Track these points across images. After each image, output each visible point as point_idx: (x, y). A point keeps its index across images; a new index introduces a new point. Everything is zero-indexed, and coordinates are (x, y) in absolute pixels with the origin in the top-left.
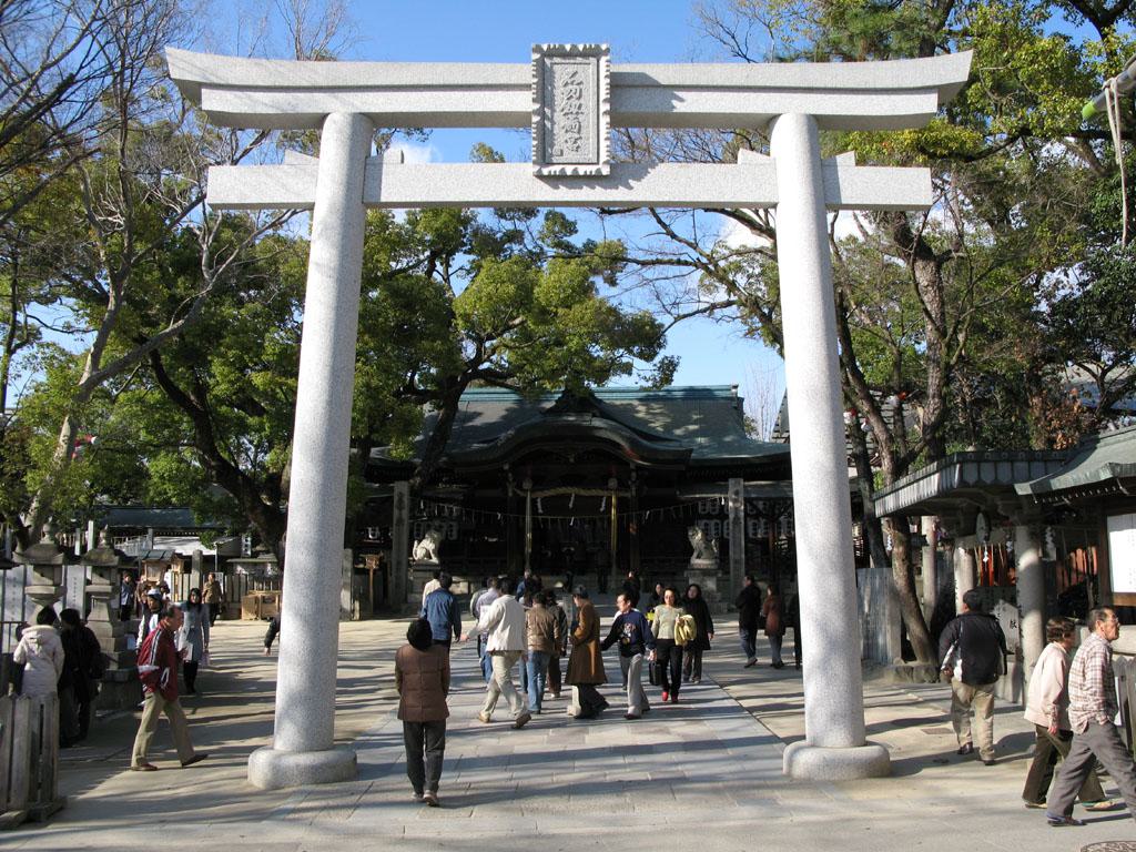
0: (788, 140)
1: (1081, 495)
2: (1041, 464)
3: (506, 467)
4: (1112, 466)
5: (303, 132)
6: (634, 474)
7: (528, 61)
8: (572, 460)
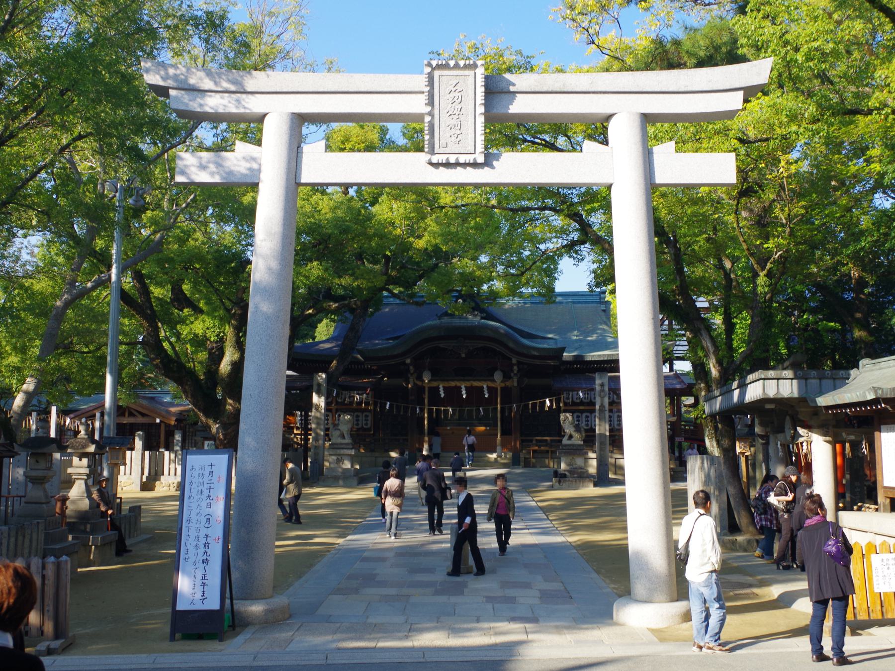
0: (624, 132)
1: (856, 409)
2: (831, 382)
3: (408, 361)
4: (875, 389)
6: (515, 368)
7: (421, 73)
8: (463, 355)
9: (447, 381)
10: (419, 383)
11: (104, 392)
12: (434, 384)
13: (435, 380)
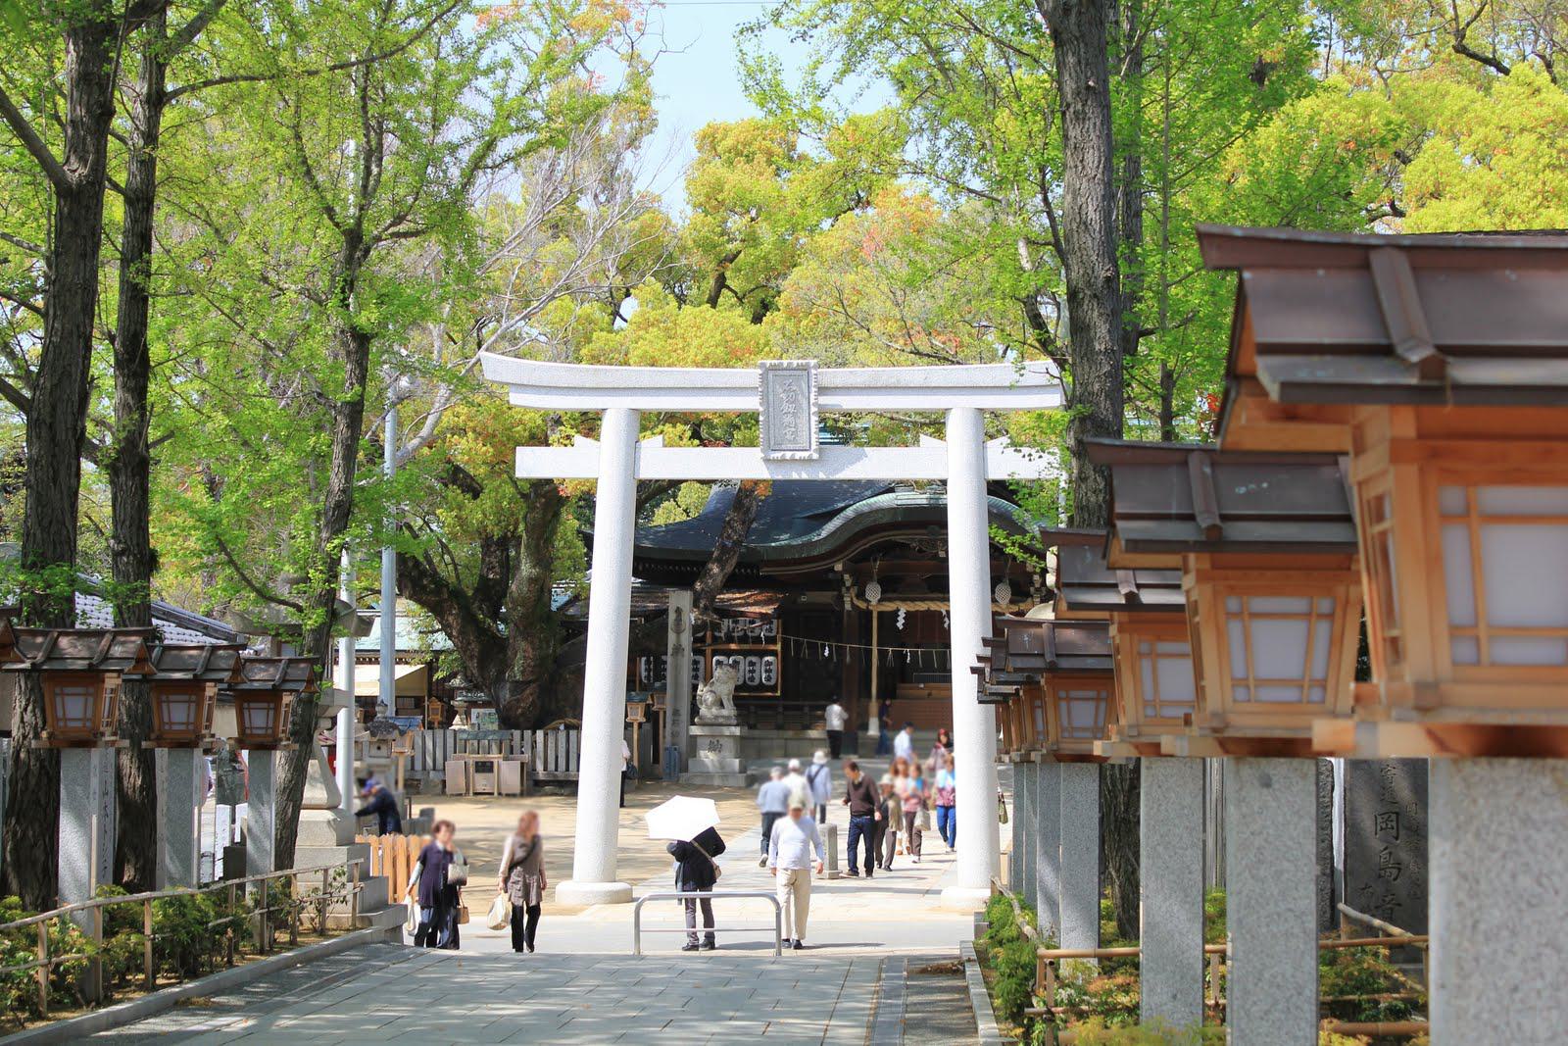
5: (589, 424)
9: (913, 600)
10: (862, 605)
11: (940, 586)
12: (889, 607)
13: (890, 600)
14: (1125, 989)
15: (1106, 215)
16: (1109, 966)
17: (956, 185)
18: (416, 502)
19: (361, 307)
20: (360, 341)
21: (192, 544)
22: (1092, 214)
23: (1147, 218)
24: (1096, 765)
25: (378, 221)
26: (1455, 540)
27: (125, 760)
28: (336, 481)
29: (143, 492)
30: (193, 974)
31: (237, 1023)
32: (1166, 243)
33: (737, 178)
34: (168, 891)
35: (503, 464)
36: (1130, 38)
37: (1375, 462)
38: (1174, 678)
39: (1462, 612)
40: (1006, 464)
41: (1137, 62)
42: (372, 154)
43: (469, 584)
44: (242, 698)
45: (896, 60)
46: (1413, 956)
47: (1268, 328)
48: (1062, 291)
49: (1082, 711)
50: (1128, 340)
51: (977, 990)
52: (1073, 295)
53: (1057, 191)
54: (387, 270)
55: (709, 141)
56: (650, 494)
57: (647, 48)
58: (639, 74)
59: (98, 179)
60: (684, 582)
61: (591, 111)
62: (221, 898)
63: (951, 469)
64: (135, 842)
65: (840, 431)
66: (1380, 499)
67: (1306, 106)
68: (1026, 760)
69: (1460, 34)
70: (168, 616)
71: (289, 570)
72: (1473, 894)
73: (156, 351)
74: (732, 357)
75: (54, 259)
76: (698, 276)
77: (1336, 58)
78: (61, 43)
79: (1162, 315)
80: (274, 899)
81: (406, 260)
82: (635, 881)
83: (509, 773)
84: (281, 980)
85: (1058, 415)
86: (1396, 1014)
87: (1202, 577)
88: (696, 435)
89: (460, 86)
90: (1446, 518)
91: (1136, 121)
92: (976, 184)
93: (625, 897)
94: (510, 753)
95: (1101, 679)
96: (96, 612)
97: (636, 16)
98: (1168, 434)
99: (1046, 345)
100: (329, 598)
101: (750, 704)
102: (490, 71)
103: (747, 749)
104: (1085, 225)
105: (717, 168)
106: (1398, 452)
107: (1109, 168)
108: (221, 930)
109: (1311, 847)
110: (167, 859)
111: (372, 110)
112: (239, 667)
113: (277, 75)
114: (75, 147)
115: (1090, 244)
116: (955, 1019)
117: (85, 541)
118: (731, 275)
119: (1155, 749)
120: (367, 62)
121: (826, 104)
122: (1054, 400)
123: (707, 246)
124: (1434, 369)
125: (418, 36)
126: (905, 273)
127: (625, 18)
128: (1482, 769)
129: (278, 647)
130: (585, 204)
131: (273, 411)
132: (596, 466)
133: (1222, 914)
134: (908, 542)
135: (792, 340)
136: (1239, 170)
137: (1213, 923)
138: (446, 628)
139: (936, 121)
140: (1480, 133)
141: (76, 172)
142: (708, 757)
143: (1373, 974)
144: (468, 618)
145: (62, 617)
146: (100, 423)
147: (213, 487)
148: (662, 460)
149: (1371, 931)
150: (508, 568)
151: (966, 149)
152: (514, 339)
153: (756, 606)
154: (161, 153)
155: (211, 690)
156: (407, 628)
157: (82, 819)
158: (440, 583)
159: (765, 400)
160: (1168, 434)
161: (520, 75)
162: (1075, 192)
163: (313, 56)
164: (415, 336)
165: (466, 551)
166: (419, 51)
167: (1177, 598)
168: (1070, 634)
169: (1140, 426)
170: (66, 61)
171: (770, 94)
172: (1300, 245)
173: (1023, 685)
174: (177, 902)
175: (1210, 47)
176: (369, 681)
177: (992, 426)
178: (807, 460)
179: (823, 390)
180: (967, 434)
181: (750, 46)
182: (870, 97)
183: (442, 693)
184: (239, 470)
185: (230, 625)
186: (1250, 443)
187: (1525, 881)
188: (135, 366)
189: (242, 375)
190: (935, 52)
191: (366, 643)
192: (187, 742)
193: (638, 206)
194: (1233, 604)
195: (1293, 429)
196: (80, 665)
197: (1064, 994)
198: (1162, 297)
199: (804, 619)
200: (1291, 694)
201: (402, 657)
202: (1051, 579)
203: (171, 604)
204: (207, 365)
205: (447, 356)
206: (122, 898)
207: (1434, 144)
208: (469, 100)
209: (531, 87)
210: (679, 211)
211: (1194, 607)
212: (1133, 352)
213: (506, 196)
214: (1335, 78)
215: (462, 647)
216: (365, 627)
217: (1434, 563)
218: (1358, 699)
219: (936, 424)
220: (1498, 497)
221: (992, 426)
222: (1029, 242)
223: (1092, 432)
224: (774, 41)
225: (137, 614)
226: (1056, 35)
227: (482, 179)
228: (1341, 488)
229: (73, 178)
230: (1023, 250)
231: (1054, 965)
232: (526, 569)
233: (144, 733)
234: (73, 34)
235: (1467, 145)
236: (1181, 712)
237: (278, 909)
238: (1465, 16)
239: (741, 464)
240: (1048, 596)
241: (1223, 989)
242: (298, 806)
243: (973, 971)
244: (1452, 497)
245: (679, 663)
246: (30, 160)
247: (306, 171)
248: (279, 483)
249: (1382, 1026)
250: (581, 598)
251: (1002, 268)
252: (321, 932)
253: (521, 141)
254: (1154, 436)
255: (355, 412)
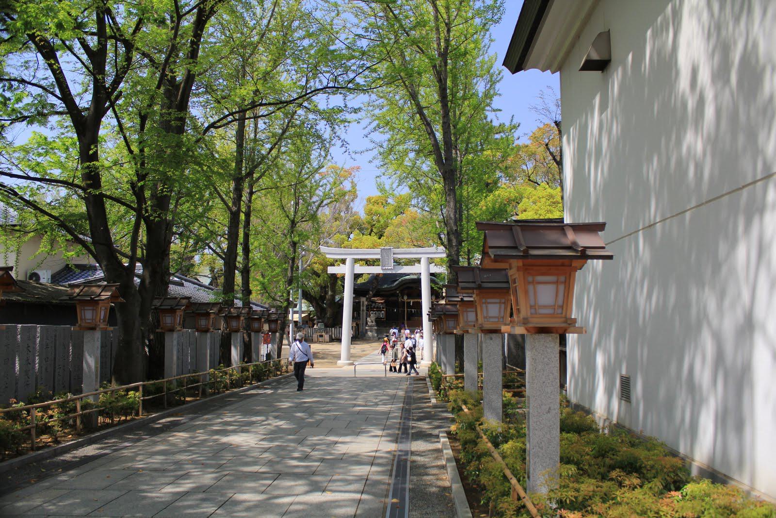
5: (343, 261)
11: (419, 296)
12: (409, 300)
14: (461, 383)
15: (455, 216)
16: (457, 378)
17: (422, 209)
18: (306, 278)
19: (294, 237)
20: (294, 244)
21: (258, 288)
22: (452, 216)
23: (464, 216)
24: (454, 339)
25: (298, 218)
26: (531, 288)
27: (245, 335)
28: (289, 274)
29: (248, 278)
30: (260, 381)
31: (269, 392)
32: (468, 222)
33: (375, 208)
34: (254, 363)
35: (325, 270)
36: (459, 178)
37: (514, 272)
38: (471, 316)
39: (532, 303)
40: (434, 269)
41: (461, 182)
42: (297, 204)
43: (318, 297)
44: (269, 321)
45: (410, 183)
46: (522, 375)
47: (491, 243)
48: (446, 232)
49: (451, 323)
50: (460, 243)
51: (429, 384)
52: (448, 234)
53: (444, 211)
54: (300, 229)
55: (369, 200)
56: (357, 276)
57: (355, 180)
58: (354, 186)
59: (239, 210)
60: (364, 296)
61: (344, 194)
62: (266, 365)
63: (422, 270)
64: (248, 353)
65: (398, 262)
66: (515, 279)
67: (497, 193)
68: (439, 334)
69: (529, 177)
70: (254, 304)
71: (279, 294)
72: (535, 363)
73: (251, 247)
74: (374, 247)
75: (230, 228)
76: (367, 229)
77: (504, 182)
78: (231, 182)
79: (467, 238)
80: (277, 365)
81: (304, 226)
82: (354, 361)
83: (327, 337)
84: (279, 382)
85: (445, 259)
86: (519, 387)
87: (477, 295)
88: (366, 263)
89: (316, 189)
90: (529, 283)
91: (461, 196)
92: (427, 209)
93: (352, 364)
94: (327, 333)
95: (455, 316)
96: (239, 303)
97: (353, 174)
98: (469, 263)
99: (442, 244)
100: (288, 300)
101: (379, 322)
102: (322, 186)
103: (378, 332)
104: (451, 218)
105: (371, 206)
106: (518, 269)
107: (455, 206)
108: (266, 371)
109: (501, 353)
110: (254, 356)
111: (297, 195)
112: (269, 315)
113: (277, 188)
114: (234, 203)
115: (452, 222)
116: (425, 390)
117: (236, 287)
118: (375, 228)
119: (467, 332)
120: (296, 185)
121: (395, 192)
122: (444, 255)
123: (369, 223)
124: (526, 251)
125: (307, 179)
126: (412, 228)
127: (351, 174)
128: (536, 336)
129: (277, 310)
130: (342, 214)
131: (276, 260)
132: (345, 270)
133: (482, 366)
134: (413, 286)
135: (387, 243)
136: (482, 206)
137: (480, 368)
138: (313, 306)
139: (417, 196)
140: (534, 197)
141: (234, 209)
142: (370, 334)
143: (514, 379)
144: (317, 303)
145: (232, 304)
146: (239, 262)
147: (263, 276)
148: (359, 269)
149: (513, 369)
150: (326, 293)
151: (425, 202)
152: (327, 243)
153: (379, 301)
154: (252, 205)
155: (263, 320)
156: (305, 306)
157: (236, 347)
158: (311, 296)
159: (382, 256)
160: (469, 263)
161: (329, 187)
162: (448, 211)
163: (285, 184)
164: (306, 243)
165: (317, 289)
166: (307, 182)
167: (472, 299)
168: (448, 307)
169: (463, 262)
170: (232, 185)
171: (382, 190)
172: (499, 225)
173: (439, 317)
174: (256, 365)
175: (477, 180)
176: (296, 317)
177: (431, 261)
178: (390, 268)
179: (394, 254)
180: (426, 263)
181: (378, 179)
182: (404, 191)
183: (312, 320)
184: (269, 272)
185: (267, 306)
186: (487, 267)
187: (546, 360)
188: (246, 250)
189: (269, 252)
190: (418, 181)
191: (295, 309)
192: (258, 331)
193: (353, 215)
194: (484, 301)
195: (497, 264)
196: (235, 315)
197: (448, 384)
198: (467, 233)
199: (389, 304)
200: (496, 320)
201: (303, 312)
202: (444, 294)
203: (254, 301)
204: (262, 250)
205: (313, 247)
206: (245, 365)
207: (524, 200)
208: (317, 192)
209: (331, 189)
210: (363, 215)
211: (476, 301)
212: (461, 245)
213: (325, 213)
214: (503, 186)
215: (316, 310)
216: (295, 306)
217: (526, 293)
218: (511, 321)
219: (419, 261)
220: (540, 278)
221: (431, 261)
222: (439, 222)
223: (452, 263)
224: (384, 179)
225: (247, 303)
226: (444, 178)
227: (320, 209)
228: (507, 275)
229: (234, 210)
230: (437, 223)
231: (446, 378)
232: (330, 293)
233: (249, 329)
234: (234, 180)
235: (531, 200)
236: (473, 324)
237: (278, 367)
238: (530, 172)
239: (376, 270)
240: (443, 298)
241: (482, 383)
242: (282, 345)
243: (428, 379)
244: (530, 279)
245: (363, 314)
246: (225, 206)
247: (282, 207)
248: (278, 275)
249: (516, 390)
250: (342, 299)
251: (433, 227)
252: (287, 372)
253: (329, 201)
254: (466, 264)
255: (293, 259)
